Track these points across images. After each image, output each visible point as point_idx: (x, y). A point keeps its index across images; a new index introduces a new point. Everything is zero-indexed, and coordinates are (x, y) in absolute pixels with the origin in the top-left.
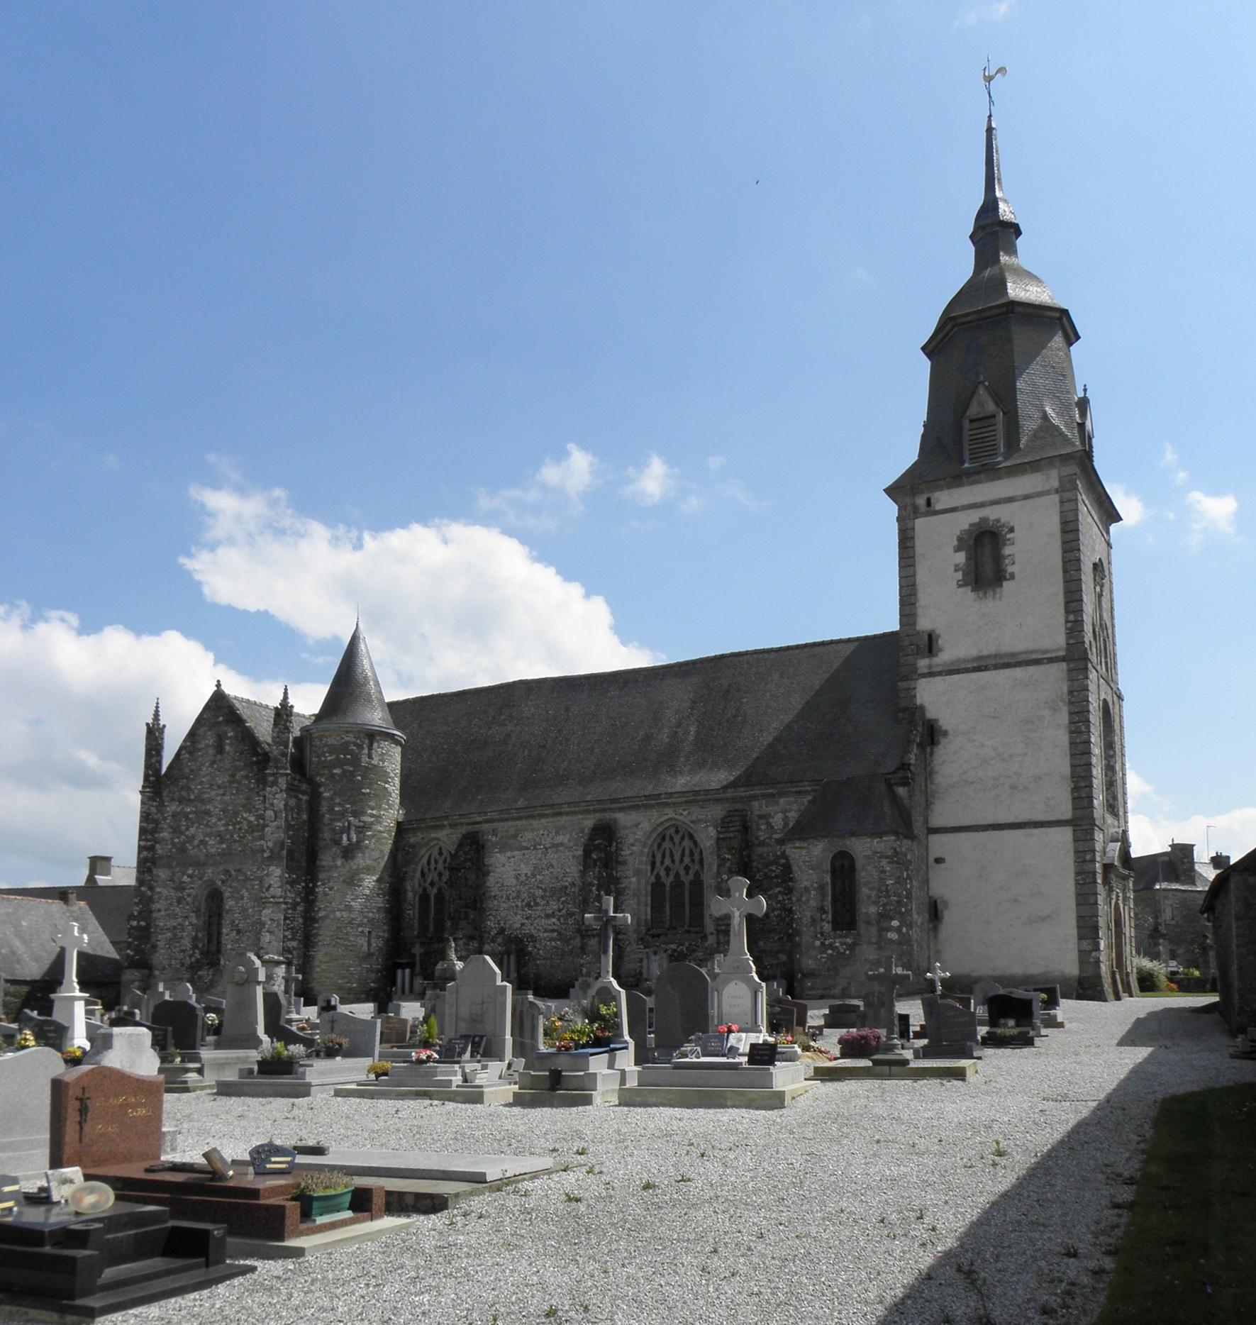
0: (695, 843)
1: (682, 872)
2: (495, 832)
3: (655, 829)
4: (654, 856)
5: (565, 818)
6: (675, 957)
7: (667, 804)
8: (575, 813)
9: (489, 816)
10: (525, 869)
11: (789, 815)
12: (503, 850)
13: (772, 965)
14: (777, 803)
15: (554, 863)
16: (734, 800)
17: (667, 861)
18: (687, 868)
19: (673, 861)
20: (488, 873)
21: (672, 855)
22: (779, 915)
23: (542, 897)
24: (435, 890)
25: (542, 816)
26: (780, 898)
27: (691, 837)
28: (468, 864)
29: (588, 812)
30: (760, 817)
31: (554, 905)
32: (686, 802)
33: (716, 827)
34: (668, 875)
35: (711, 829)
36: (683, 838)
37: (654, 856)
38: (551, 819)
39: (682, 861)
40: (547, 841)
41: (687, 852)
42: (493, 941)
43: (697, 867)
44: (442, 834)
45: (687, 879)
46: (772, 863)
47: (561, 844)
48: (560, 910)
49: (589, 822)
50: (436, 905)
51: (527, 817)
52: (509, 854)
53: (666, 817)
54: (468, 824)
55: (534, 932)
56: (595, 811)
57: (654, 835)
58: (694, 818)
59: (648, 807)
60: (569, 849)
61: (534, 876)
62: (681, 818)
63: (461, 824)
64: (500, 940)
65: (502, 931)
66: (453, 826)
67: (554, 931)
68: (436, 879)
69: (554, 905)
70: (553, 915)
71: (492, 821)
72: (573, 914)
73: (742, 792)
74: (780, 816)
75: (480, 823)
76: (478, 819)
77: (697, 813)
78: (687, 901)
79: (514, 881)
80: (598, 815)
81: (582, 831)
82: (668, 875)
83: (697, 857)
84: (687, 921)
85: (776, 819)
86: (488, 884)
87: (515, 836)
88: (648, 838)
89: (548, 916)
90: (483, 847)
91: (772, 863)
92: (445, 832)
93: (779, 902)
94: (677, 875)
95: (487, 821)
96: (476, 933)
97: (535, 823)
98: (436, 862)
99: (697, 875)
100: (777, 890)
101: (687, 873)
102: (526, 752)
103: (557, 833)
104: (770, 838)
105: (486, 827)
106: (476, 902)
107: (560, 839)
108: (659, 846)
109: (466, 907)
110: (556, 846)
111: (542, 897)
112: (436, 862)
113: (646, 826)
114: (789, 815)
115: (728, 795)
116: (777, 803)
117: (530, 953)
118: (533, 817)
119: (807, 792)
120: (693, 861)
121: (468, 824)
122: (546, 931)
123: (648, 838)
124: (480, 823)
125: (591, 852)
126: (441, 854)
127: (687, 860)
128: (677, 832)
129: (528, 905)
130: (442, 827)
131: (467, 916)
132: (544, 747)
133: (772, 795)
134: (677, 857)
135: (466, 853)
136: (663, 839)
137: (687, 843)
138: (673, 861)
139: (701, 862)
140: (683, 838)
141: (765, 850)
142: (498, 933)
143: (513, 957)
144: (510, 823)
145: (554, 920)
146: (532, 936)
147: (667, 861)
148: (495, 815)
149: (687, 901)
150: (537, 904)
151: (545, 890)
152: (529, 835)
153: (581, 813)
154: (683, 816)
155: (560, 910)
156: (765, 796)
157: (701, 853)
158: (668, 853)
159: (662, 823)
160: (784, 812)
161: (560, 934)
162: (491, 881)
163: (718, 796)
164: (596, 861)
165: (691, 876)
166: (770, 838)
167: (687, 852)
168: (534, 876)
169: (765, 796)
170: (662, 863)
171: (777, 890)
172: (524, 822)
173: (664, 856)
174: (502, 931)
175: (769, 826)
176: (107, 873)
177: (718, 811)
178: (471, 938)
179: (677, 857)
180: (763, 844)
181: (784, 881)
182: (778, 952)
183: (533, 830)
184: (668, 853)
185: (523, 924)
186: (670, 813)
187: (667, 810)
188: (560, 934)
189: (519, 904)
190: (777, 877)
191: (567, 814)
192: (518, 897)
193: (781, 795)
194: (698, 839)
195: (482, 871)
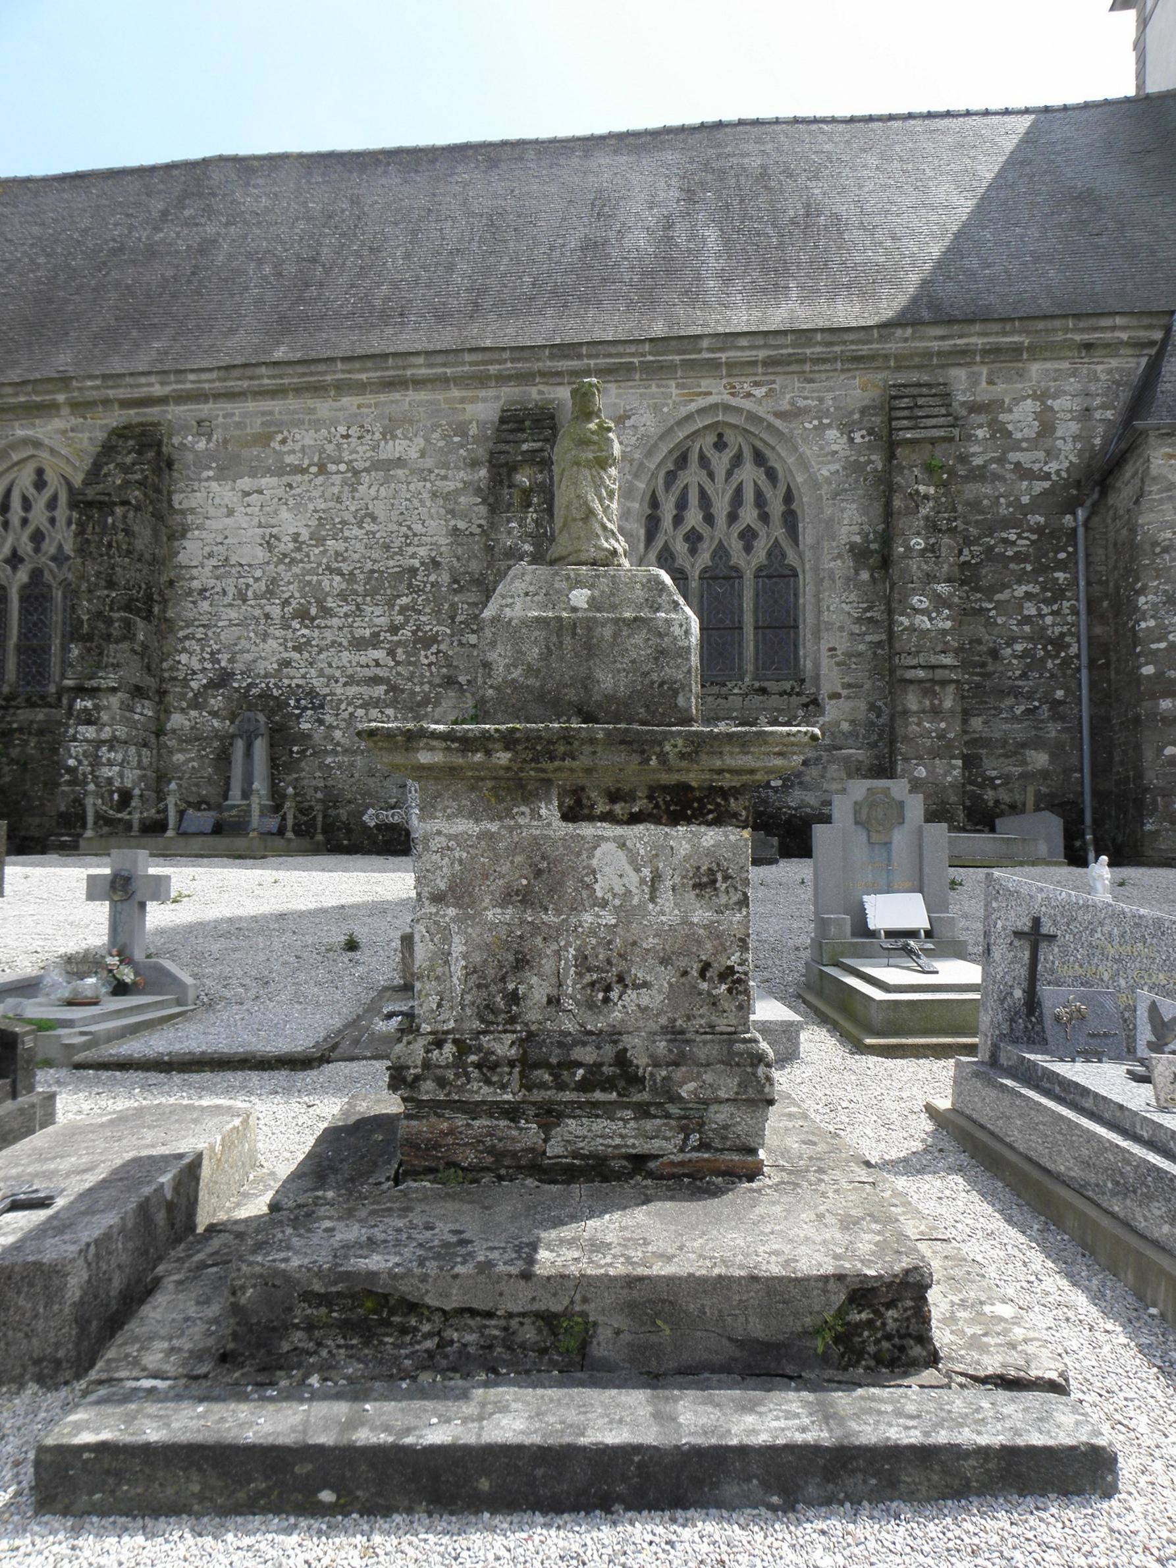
0: (771, 475)
1: (735, 546)
2: (203, 427)
3: (670, 431)
4: (654, 503)
5: (413, 395)
6: (210, 779)
7: (714, 365)
8: (444, 381)
9: (190, 383)
10: (290, 523)
11: (1056, 404)
12: (227, 470)
13: (1007, 778)
14: (1021, 374)
15: (379, 509)
16: (902, 362)
17: (694, 517)
18: (748, 536)
19: (709, 519)
20: (183, 532)
21: (705, 501)
22: (1026, 653)
23: (343, 596)
24: (22, 576)
25: (342, 388)
26: (1030, 610)
27: (759, 458)
28: (135, 495)
29: (482, 380)
30: (975, 408)
31: (377, 616)
32: (769, 363)
33: (847, 429)
34: (693, 551)
35: (832, 434)
36: (737, 461)
37: (654, 503)
38: (370, 399)
39: (733, 517)
40: (361, 454)
41: (749, 495)
42: (196, 705)
43: (779, 532)
44: (48, 430)
45: (749, 563)
46: (1006, 523)
47: (400, 462)
48: (394, 629)
49: (483, 408)
50: (24, 612)
51: (298, 391)
52: (245, 483)
53: (702, 402)
54: (126, 404)
55: (318, 683)
56: (502, 379)
57: (664, 449)
58: (785, 405)
59: (655, 371)
60: (423, 474)
61: (320, 541)
62: (747, 404)
63: (106, 402)
64: (216, 702)
65: (222, 679)
66: (78, 407)
67: (375, 680)
68: (26, 547)
69: (377, 616)
70: (374, 641)
71: (200, 397)
72: (434, 639)
73: (933, 340)
74: (1029, 405)
75: (163, 401)
76: (158, 390)
77: (792, 391)
78: (748, 620)
79: (261, 554)
80: (509, 393)
81: (461, 429)
82: (693, 551)
83: (776, 508)
84: (750, 667)
85: (1017, 414)
86: (182, 558)
87: (264, 439)
88: (649, 454)
89: (359, 644)
90: (170, 464)
91: (1006, 523)
92: (57, 423)
93: (1027, 620)
94: (721, 551)
95: (182, 398)
96: (150, 682)
97: (324, 407)
98: (27, 505)
99: (775, 551)
100: (1020, 591)
101: (748, 549)
102: (267, 269)
103: (388, 434)
104: (1001, 461)
105: (175, 412)
106: (146, 601)
107: (392, 449)
108: (671, 477)
109: (128, 608)
110: (386, 466)
111: (343, 596)
112: (27, 505)
113: (647, 421)
114: (1056, 404)
115: (891, 347)
116: (1021, 374)
117: (306, 737)
118: (317, 389)
119: (1112, 348)
120: (764, 517)
121: (126, 404)
122: (351, 681)
123: (649, 454)
124: (163, 401)
125: (513, 468)
126: (40, 483)
127: (749, 515)
128: (720, 445)
129: (303, 615)
130: (48, 409)
131: (128, 634)
132: (314, 260)
133: (1016, 351)
134: (721, 508)
135: (125, 469)
136: (682, 461)
137: (749, 474)
138: (709, 519)
139: (791, 520)
140: (737, 461)
141: (987, 489)
142: (213, 685)
143: (260, 747)
144: (251, 405)
145: (379, 654)
146: (312, 693)
147: (694, 517)
148: (210, 382)
149: (748, 620)
150: (327, 612)
151: (351, 578)
152: (308, 438)
153: (458, 381)
154: (756, 398)
155: (394, 629)
156: (993, 353)
157: (789, 498)
158: (693, 498)
159: (689, 418)
160: (1041, 396)
161: (393, 688)
162: (191, 551)
163: (864, 349)
164: (527, 493)
165: (760, 554)
166: (1001, 461)
167: (749, 495)
168: (320, 541)
169: (993, 353)
170: (678, 520)
171: (1020, 591)
172: (293, 403)
173: (682, 505)
174: (222, 679)
175: (1000, 431)
176: (91, 879)
177: (857, 390)
178: (138, 692)
179: (721, 508)
180: (979, 475)
181: (1041, 569)
182: (1024, 745)
183: (317, 424)
184: (693, 498)
185: (286, 663)
186: (716, 391)
187: (705, 384)
188: (393, 688)
189: (276, 611)
190: (1019, 558)
191: (419, 383)
192: (270, 593)
193: (1035, 352)
194: (773, 463)
195: (169, 526)
